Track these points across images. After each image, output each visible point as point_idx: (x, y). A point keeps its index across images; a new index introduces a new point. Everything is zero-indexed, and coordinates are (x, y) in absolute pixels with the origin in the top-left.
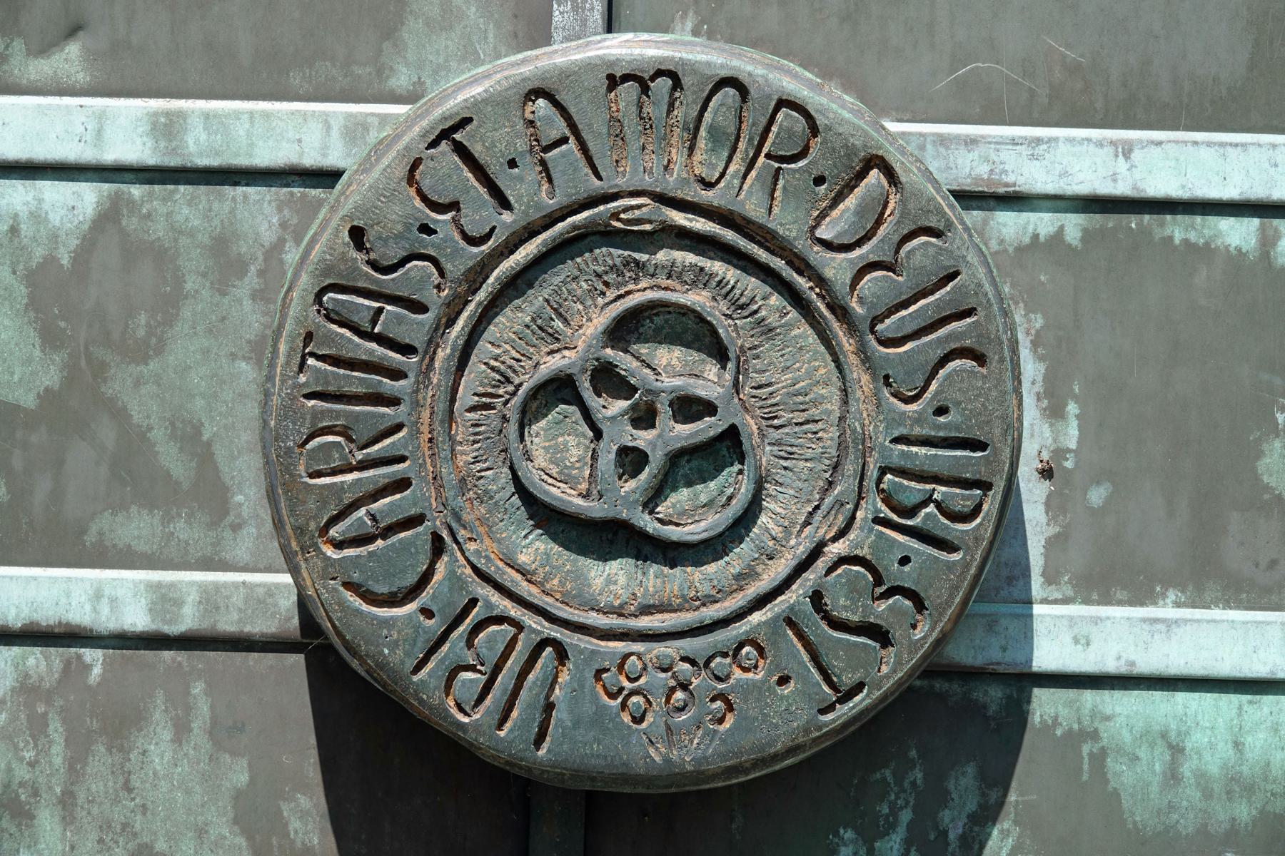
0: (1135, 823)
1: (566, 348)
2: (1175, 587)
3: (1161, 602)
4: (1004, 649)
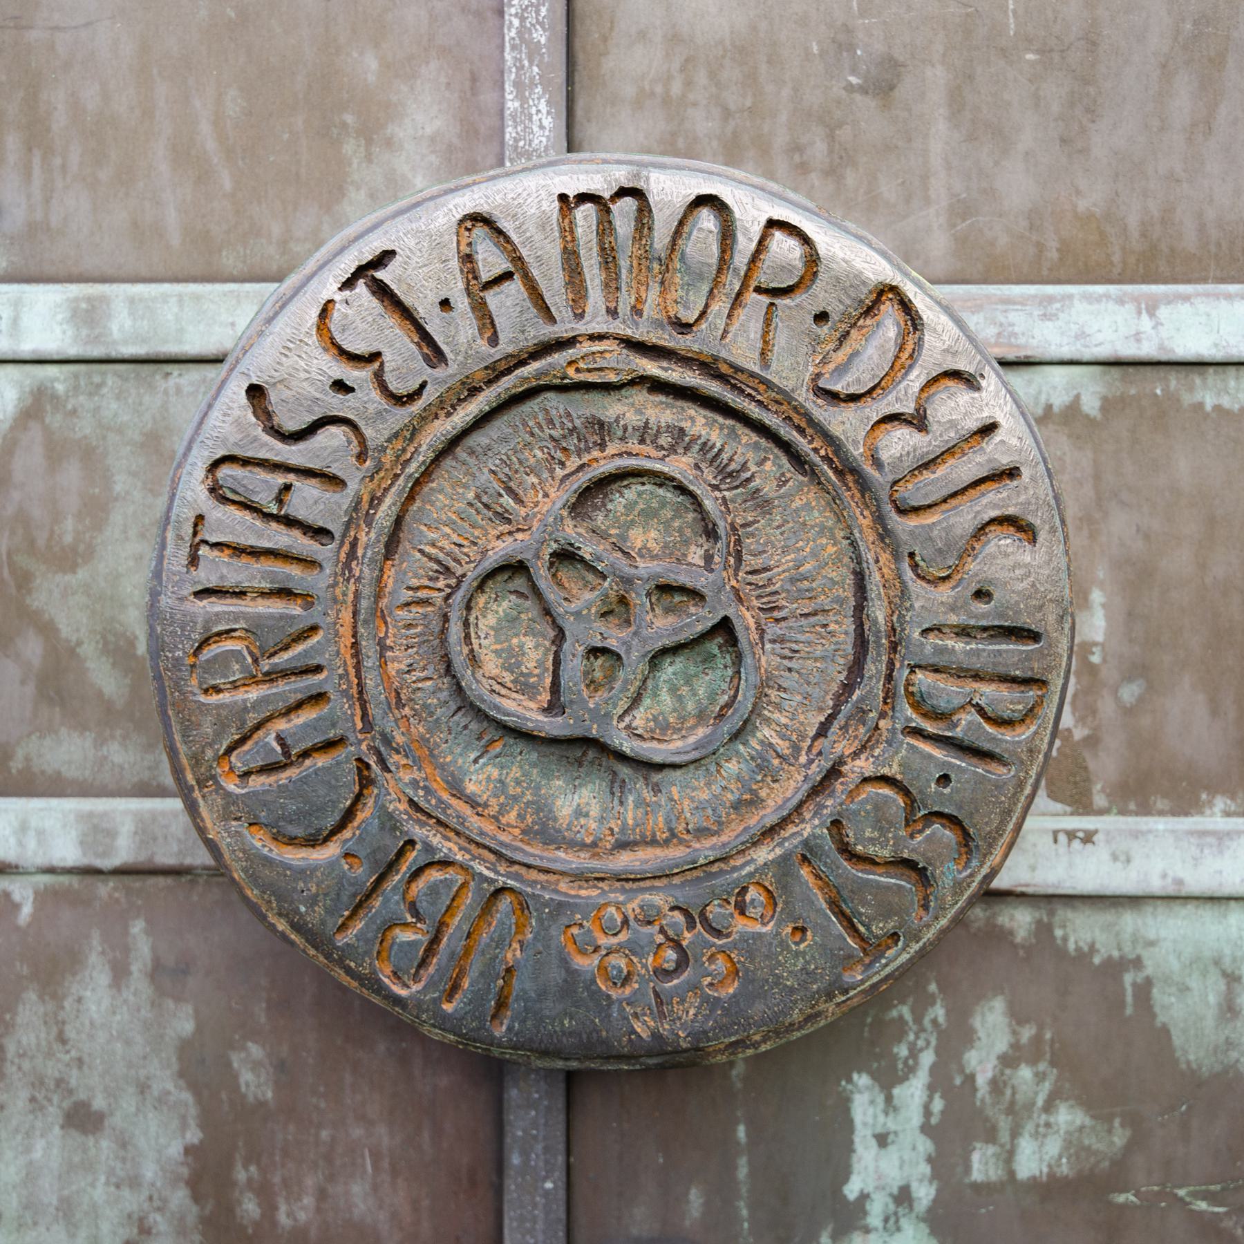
0: (1188, 1063)
1: (519, 530)
2: (1223, 793)
3: (1208, 812)
4: (1033, 868)
